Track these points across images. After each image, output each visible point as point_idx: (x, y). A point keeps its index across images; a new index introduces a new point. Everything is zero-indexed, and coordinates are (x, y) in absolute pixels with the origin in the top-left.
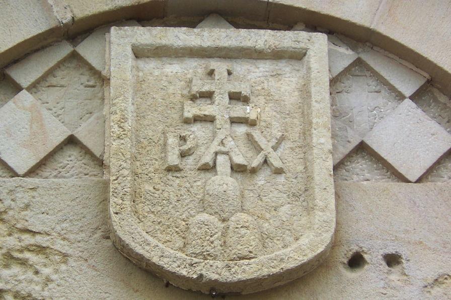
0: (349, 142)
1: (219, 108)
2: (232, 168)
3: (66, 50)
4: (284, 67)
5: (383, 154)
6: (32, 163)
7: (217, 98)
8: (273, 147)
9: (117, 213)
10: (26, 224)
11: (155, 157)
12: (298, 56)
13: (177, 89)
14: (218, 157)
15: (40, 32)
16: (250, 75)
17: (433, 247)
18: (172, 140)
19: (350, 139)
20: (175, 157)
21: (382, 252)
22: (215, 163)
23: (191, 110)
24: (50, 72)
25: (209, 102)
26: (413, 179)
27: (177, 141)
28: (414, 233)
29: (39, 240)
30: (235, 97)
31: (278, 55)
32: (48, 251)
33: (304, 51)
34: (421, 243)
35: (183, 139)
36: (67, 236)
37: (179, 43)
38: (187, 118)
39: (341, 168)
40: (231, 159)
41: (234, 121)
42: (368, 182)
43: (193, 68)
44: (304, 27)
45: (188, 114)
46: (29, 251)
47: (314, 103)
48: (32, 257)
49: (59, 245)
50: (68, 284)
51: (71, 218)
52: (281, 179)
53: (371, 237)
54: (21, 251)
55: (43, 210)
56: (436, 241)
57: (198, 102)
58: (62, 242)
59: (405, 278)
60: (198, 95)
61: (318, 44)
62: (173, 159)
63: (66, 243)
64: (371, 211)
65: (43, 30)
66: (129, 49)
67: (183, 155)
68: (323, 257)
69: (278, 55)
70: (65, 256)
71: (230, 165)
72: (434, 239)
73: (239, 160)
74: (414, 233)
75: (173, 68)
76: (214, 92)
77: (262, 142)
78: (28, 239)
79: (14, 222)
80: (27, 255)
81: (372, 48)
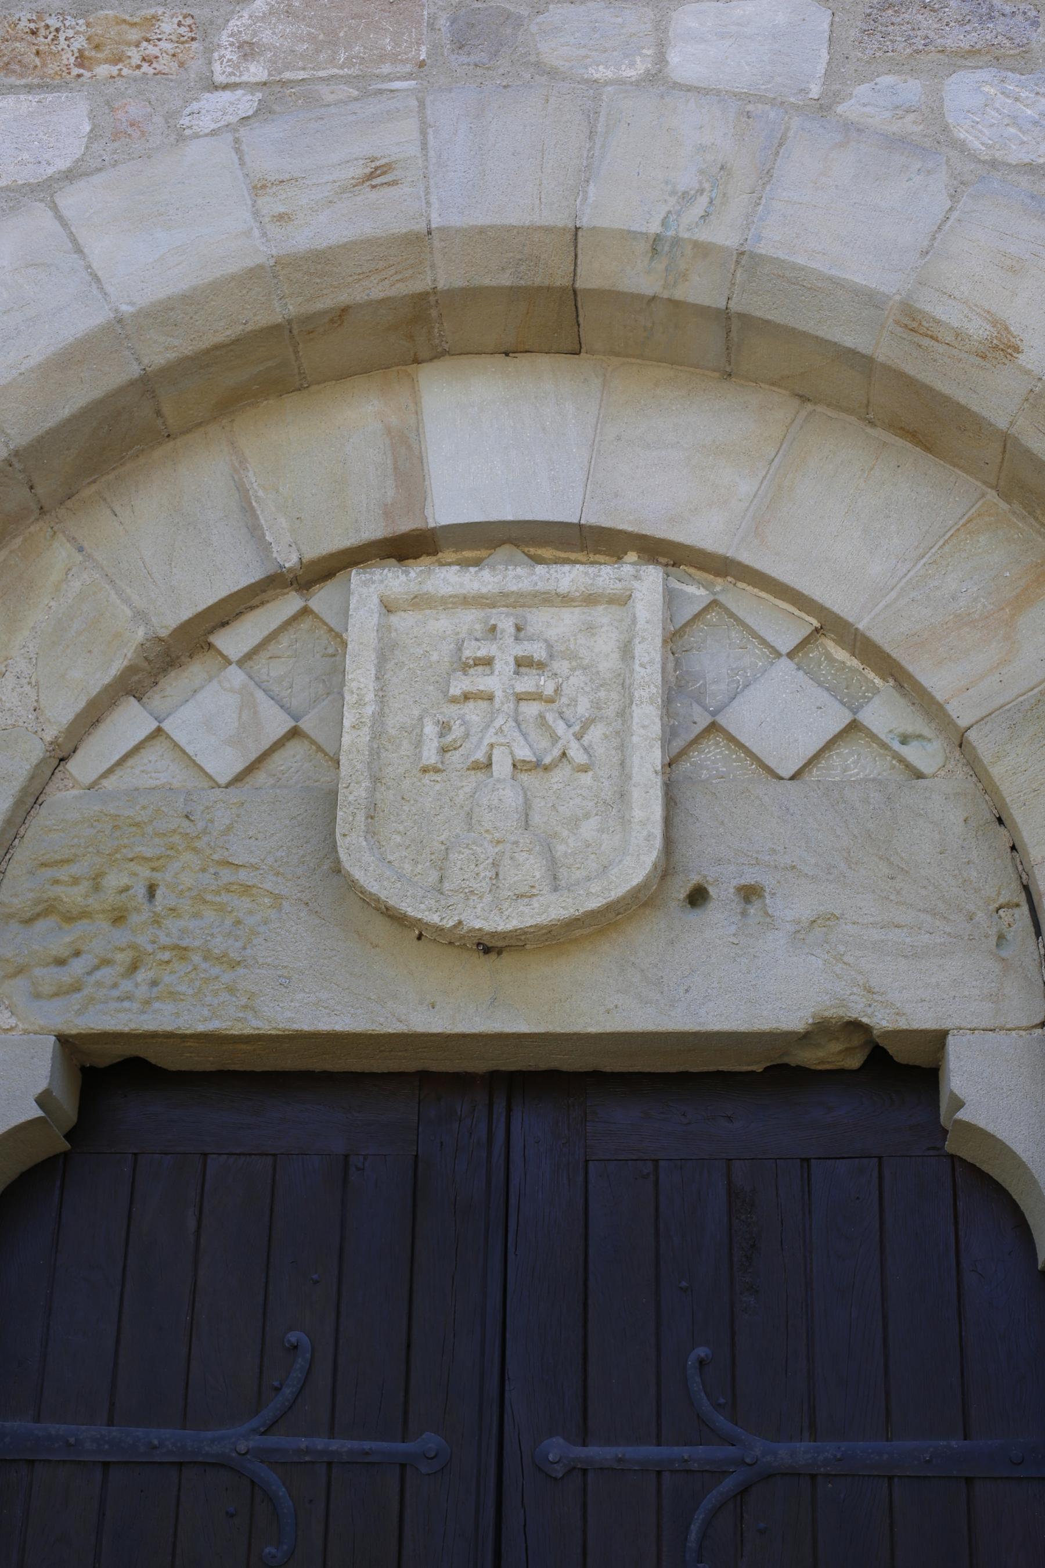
0: (695, 723)
2: (514, 766)
3: (291, 603)
4: (601, 614)
5: (743, 740)
6: (239, 767)
7: (498, 665)
8: (574, 734)
9: (345, 835)
10: (226, 853)
11: (408, 753)
12: (622, 600)
14: (495, 751)
15: (253, 581)
16: (557, 625)
17: (810, 874)
18: (430, 729)
19: (696, 719)
20: (434, 751)
21: (735, 883)
22: (490, 758)
23: (459, 686)
24: (272, 637)
26: (786, 773)
28: (785, 853)
29: (243, 875)
30: (523, 663)
31: (590, 600)
32: (254, 891)
33: (628, 593)
34: (793, 867)
36: (281, 870)
37: (445, 590)
38: (453, 696)
40: (512, 753)
43: (470, 618)
44: (636, 559)
45: (455, 690)
46: (228, 891)
47: (637, 668)
50: (279, 938)
51: (289, 844)
52: (586, 779)
53: (719, 861)
54: (217, 893)
55: (251, 833)
56: (816, 865)
57: (472, 671)
58: (274, 879)
59: (768, 920)
60: (472, 662)
61: (648, 582)
62: (430, 755)
63: (280, 879)
64: (722, 823)
65: (257, 578)
66: (375, 600)
67: (444, 750)
68: (457, 931)
69: (590, 600)
70: (278, 898)
71: (511, 762)
72: (813, 861)
73: (524, 753)
74: (785, 853)
75: (441, 624)
76: (494, 657)
77: (560, 728)
78: (227, 875)
79: (209, 852)
80: (225, 898)
81: (735, 585)
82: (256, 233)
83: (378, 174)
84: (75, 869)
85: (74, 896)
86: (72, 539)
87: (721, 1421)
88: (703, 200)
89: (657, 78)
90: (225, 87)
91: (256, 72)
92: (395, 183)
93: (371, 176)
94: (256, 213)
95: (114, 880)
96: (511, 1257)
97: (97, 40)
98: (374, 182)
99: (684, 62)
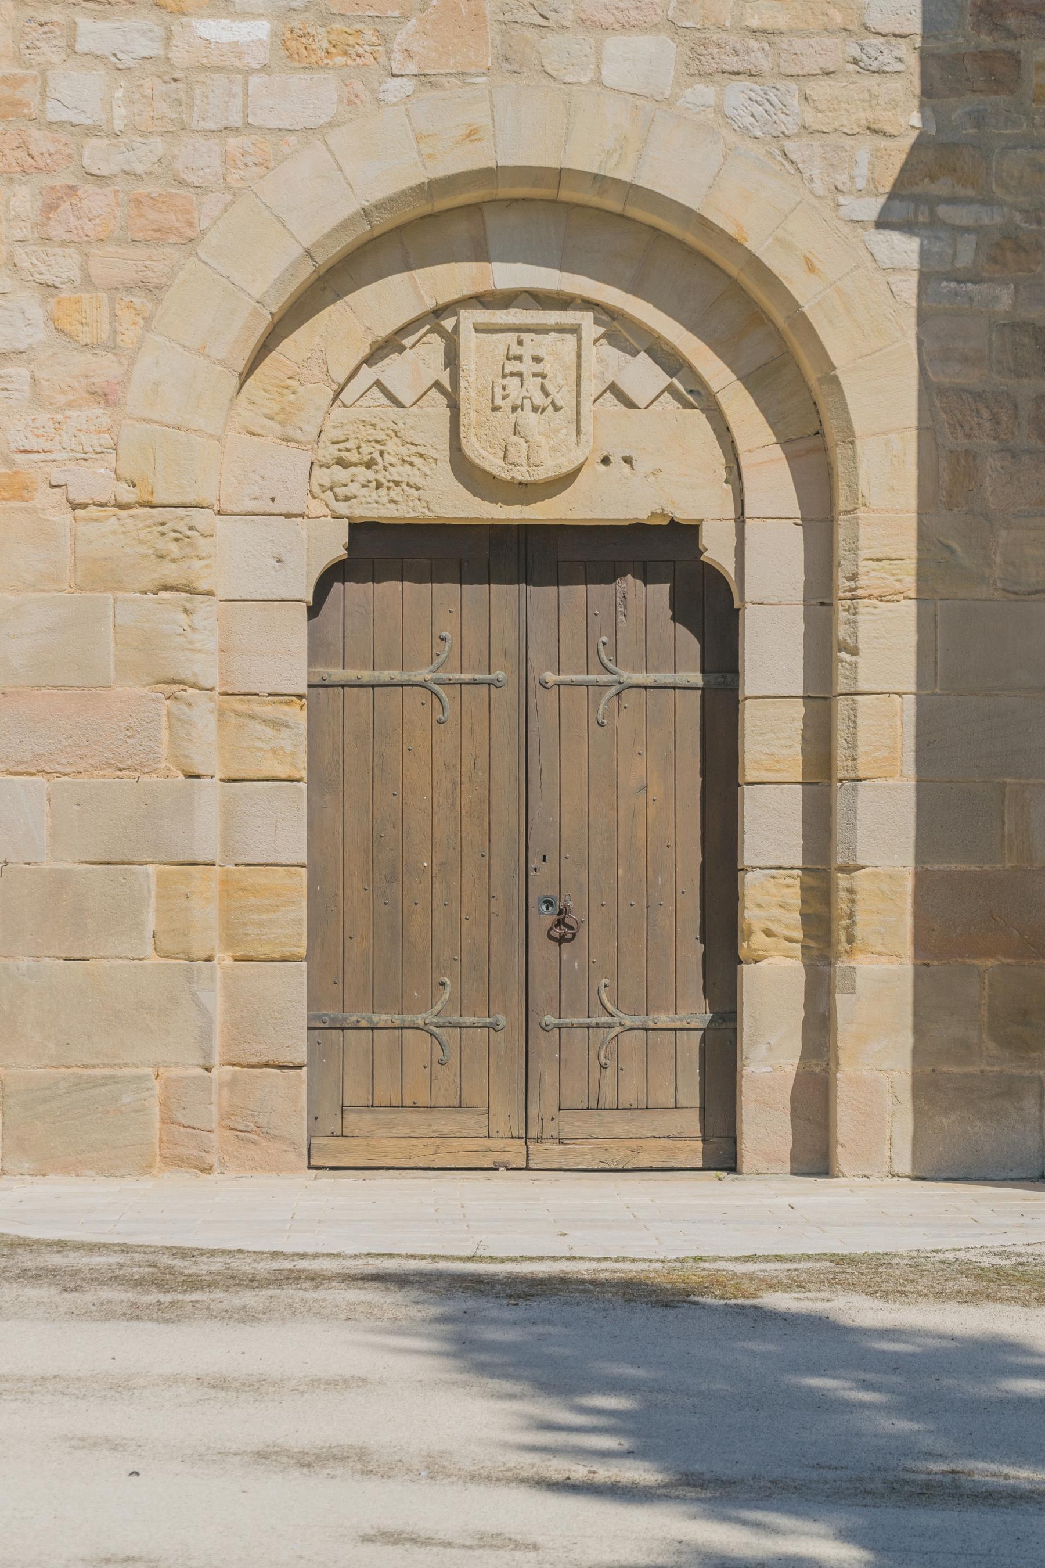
1: (527, 367)
7: (524, 359)
13: (502, 351)
23: (510, 367)
25: (963, 1477)
27: (501, 389)
29: (421, 450)
30: (537, 359)
31: (561, 330)
35: (504, 388)
39: (859, 1561)
41: (535, 375)
42: (544, 13)
43: (512, 337)
48: (417, 460)
49: (432, 453)
61: (586, 319)
69: (561, 330)
78: (414, 449)
82: (420, 164)
83: (472, 134)
84: (348, 445)
85: (353, 457)
86: (746, 698)
87: (611, 666)
88: (616, 156)
89: (598, 81)
90: (397, 76)
91: (412, 68)
92: (479, 139)
93: (469, 135)
94: (419, 152)
95: (366, 449)
96: (341, 705)
97: (334, 43)
98: (472, 138)
99: (610, 76)
